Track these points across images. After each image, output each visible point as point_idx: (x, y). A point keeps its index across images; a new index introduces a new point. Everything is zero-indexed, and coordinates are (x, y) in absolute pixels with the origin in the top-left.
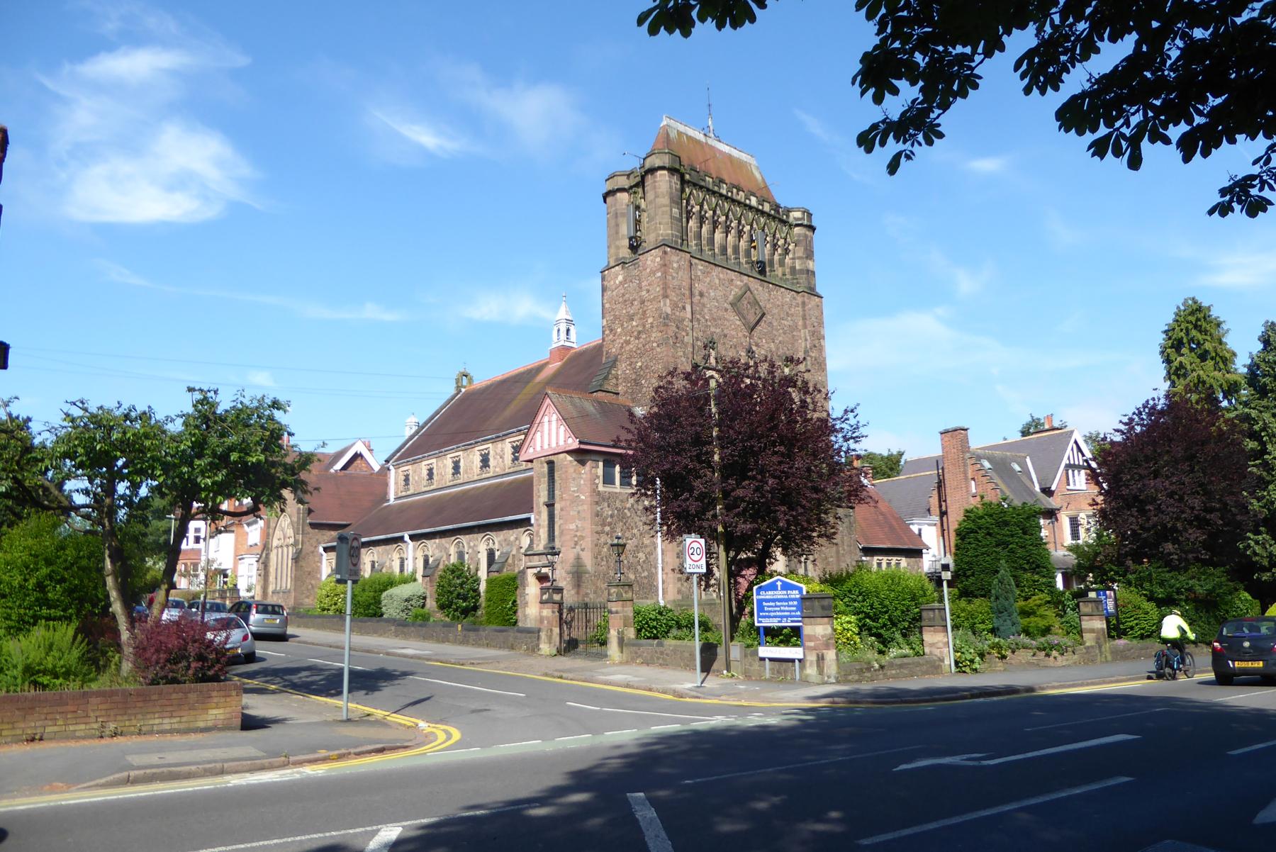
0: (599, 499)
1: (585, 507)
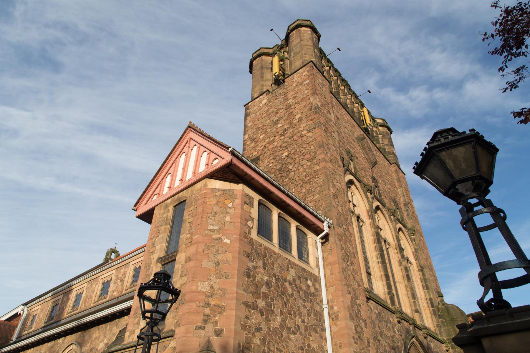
0: (251, 252)
1: (229, 256)
